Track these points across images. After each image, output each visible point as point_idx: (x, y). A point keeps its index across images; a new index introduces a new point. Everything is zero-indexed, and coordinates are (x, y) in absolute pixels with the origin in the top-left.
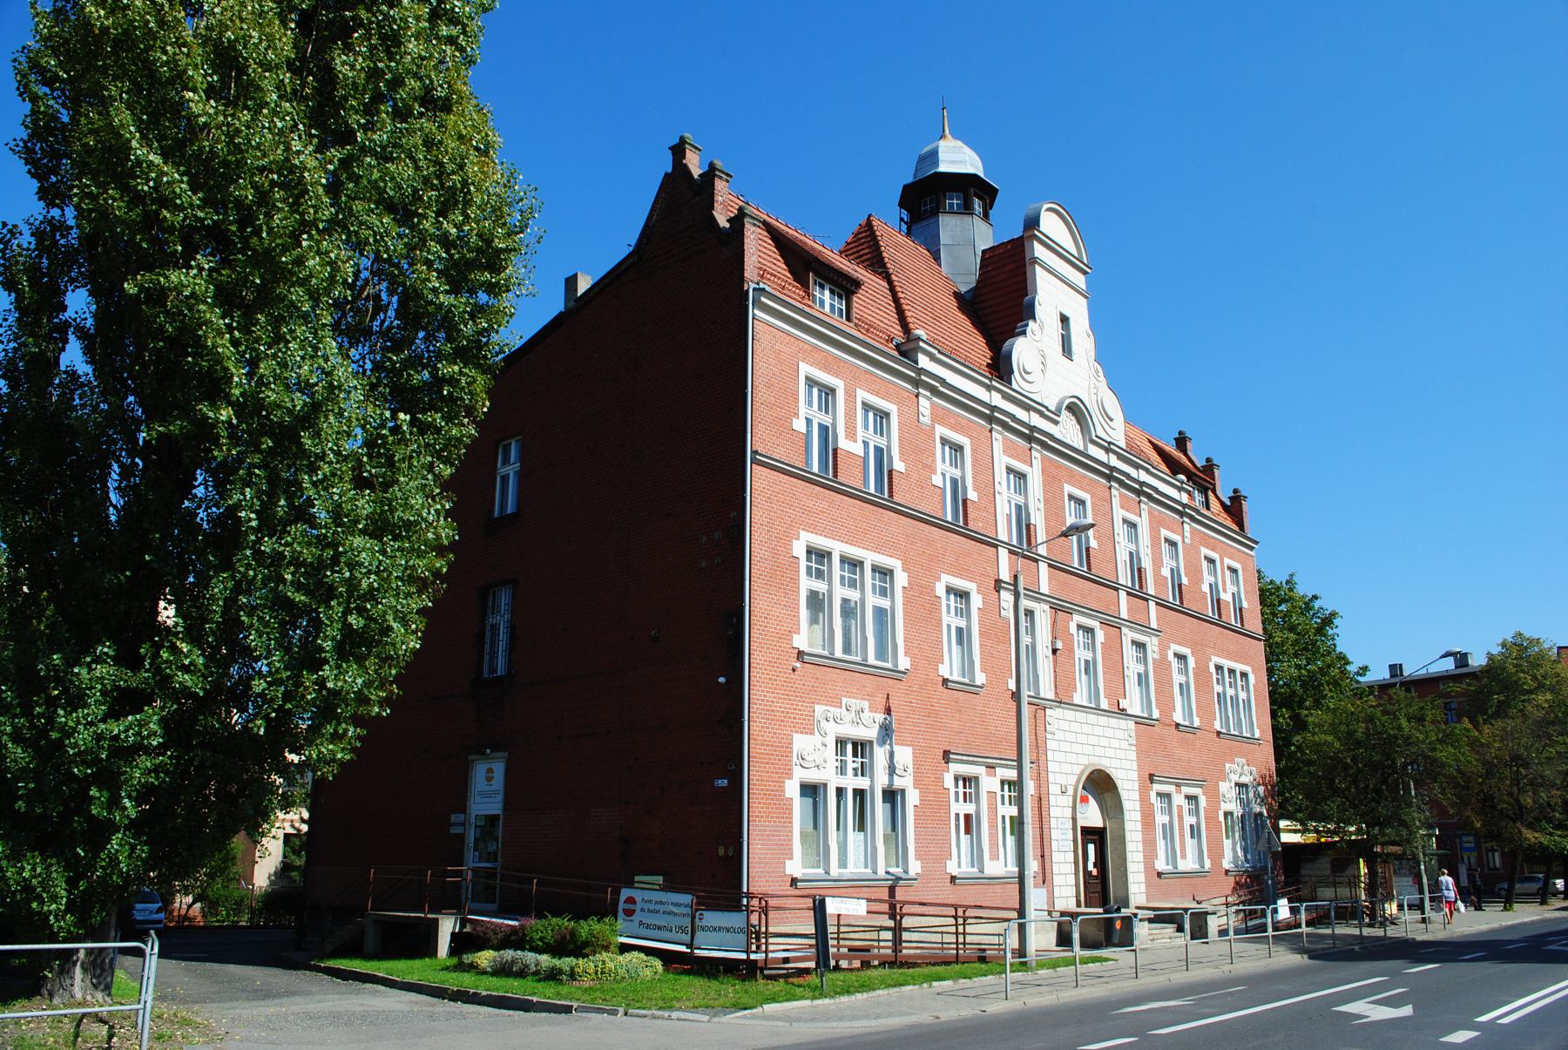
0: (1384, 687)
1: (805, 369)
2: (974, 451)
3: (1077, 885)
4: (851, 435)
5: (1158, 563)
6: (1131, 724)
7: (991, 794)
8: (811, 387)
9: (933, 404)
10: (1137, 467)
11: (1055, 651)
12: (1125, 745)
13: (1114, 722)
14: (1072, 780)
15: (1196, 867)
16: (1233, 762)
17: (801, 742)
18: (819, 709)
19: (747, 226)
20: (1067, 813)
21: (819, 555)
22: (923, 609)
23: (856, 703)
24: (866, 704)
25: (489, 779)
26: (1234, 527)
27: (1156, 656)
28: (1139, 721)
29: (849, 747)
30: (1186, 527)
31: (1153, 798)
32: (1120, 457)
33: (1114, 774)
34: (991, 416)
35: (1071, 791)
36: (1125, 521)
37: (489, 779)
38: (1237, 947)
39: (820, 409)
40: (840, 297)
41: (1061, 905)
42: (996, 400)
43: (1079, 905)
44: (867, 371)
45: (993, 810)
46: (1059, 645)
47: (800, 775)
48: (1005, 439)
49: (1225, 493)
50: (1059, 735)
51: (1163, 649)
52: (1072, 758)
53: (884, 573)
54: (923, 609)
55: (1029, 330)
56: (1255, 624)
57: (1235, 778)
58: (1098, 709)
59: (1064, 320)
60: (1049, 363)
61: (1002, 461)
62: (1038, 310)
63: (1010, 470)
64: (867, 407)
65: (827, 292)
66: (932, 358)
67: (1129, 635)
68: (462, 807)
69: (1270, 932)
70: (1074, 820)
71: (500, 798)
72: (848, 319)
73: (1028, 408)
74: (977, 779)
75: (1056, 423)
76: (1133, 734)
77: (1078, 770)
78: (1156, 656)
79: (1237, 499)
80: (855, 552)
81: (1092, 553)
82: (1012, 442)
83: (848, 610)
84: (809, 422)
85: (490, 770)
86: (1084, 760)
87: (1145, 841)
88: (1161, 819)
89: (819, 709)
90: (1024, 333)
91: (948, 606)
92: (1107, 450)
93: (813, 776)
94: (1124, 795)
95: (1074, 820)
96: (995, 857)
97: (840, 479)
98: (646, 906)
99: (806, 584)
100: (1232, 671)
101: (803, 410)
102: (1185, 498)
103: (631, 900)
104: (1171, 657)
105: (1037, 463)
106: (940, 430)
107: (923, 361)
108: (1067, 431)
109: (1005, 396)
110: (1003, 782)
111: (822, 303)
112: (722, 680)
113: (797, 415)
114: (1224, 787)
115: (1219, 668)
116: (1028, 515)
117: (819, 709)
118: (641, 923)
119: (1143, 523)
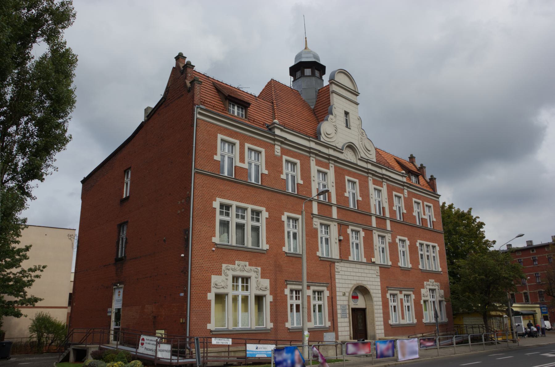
0: (505, 252)
1: (347, 178)
2: (301, 165)
3: (350, 331)
4: (242, 160)
5: (391, 204)
6: (378, 268)
7: (401, 300)
8: (319, 174)
9: (408, 191)
10: (381, 168)
11: (340, 240)
12: (375, 276)
13: (369, 267)
14: (348, 290)
15: (433, 321)
16: (428, 281)
17: (215, 279)
18: (425, 282)
19: (196, 84)
20: (343, 302)
21: (421, 245)
22: (275, 227)
23: (242, 263)
24: (247, 263)
25: (119, 295)
26: (431, 190)
27: (391, 241)
28: (383, 268)
29: (240, 280)
30: (405, 191)
31: (388, 296)
32: (372, 165)
33: (368, 287)
34: (310, 151)
35: (347, 294)
36: (375, 189)
37: (119, 295)
38: (456, 349)
39: (291, 170)
40: (242, 109)
41: (341, 339)
42: (313, 145)
43: (351, 339)
44: (250, 137)
45: (402, 303)
46: (342, 238)
47: (423, 298)
48: (373, 179)
49: (428, 177)
50: (341, 273)
51: (394, 238)
52: (349, 282)
53: (434, 247)
54: (275, 227)
55: (329, 119)
56: (440, 228)
57: (428, 287)
58: (361, 263)
59: (347, 113)
60: (339, 130)
61: (371, 186)
62: (334, 111)
63: (319, 171)
64: (427, 206)
65: (236, 108)
66: (282, 130)
67: (375, 234)
68: (111, 306)
69: (484, 342)
70: (349, 306)
71: (121, 302)
72: (419, 183)
73: (328, 148)
74: (323, 291)
75: (342, 153)
76: (379, 271)
77: (351, 286)
78: (391, 241)
79: (432, 179)
80: (428, 243)
81: (359, 202)
82: (320, 161)
83: (240, 227)
84: (287, 175)
85: (119, 292)
86: (355, 282)
87: (384, 313)
88: (391, 304)
89: (224, 266)
90: (327, 120)
91: (353, 236)
92: (367, 162)
93: (426, 299)
94: (373, 295)
95: (349, 306)
96: (309, 320)
97: (263, 184)
98: (148, 342)
99: (219, 217)
100: (428, 246)
101: (285, 171)
102: (405, 180)
103: (143, 339)
104: (397, 241)
105: (385, 187)
106: (285, 158)
107: (277, 132)
108: (349, 156)
109: (316, 143)
110: (405, 295)
111: (234, 112)
112: (183, 255)
113: (216, 154)
114: (423, 291)
115: (421, 245)
116: (382, 204)
117: (425, 282)
118: (145, 348)
119: (384, 189)
